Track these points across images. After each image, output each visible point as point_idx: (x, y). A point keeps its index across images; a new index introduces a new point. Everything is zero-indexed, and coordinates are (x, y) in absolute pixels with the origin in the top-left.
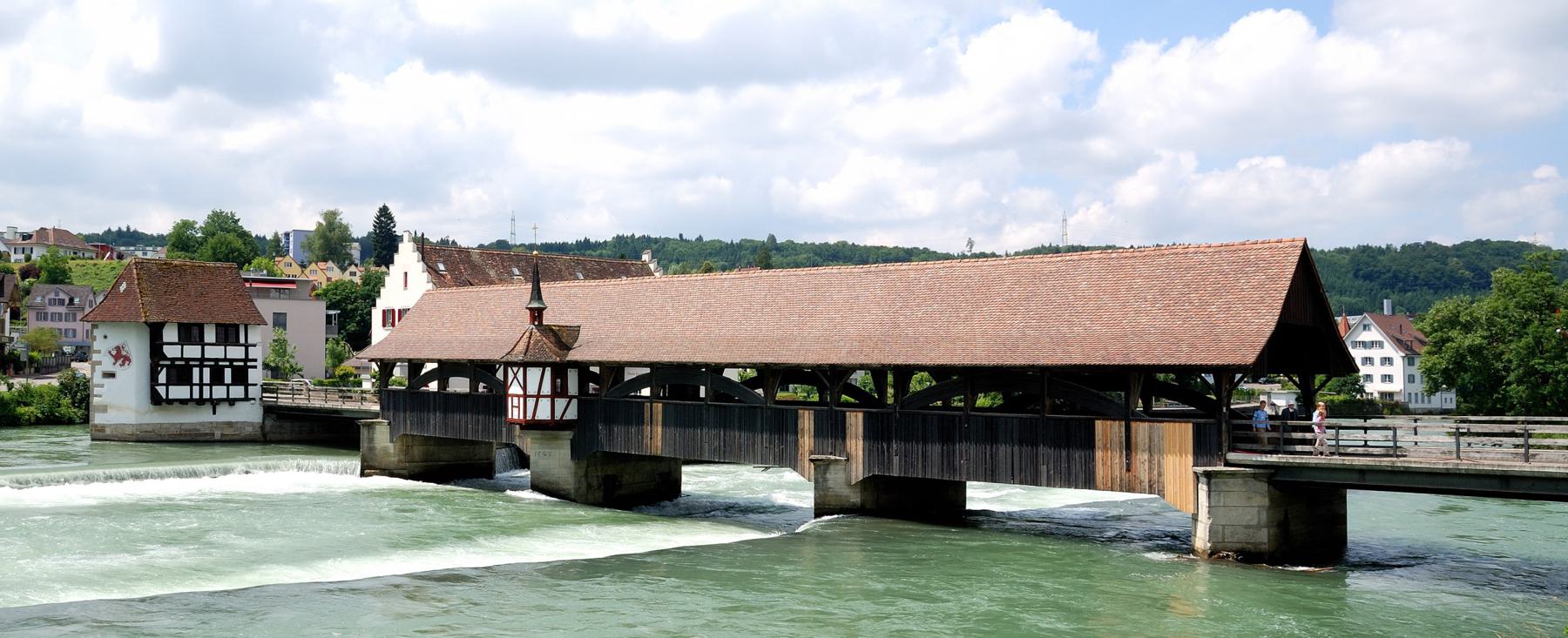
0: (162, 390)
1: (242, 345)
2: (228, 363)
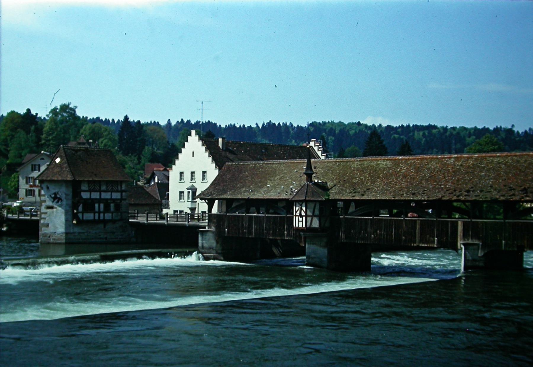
2: (112, 201)
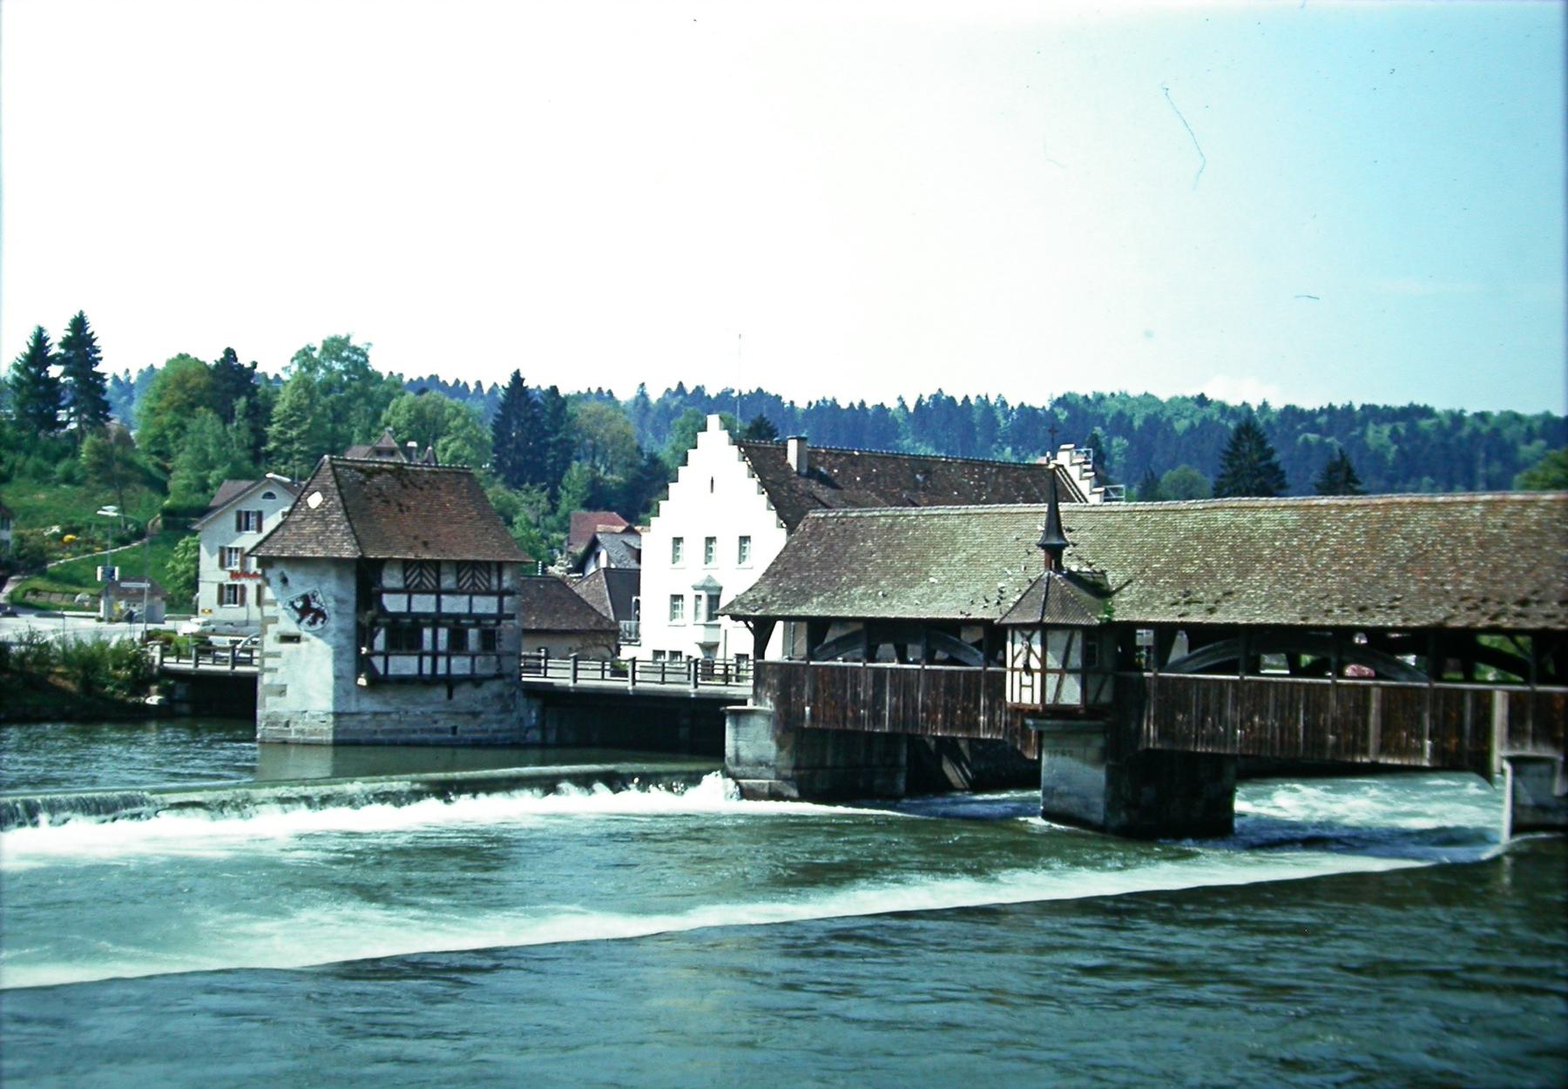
2: (472, 622)
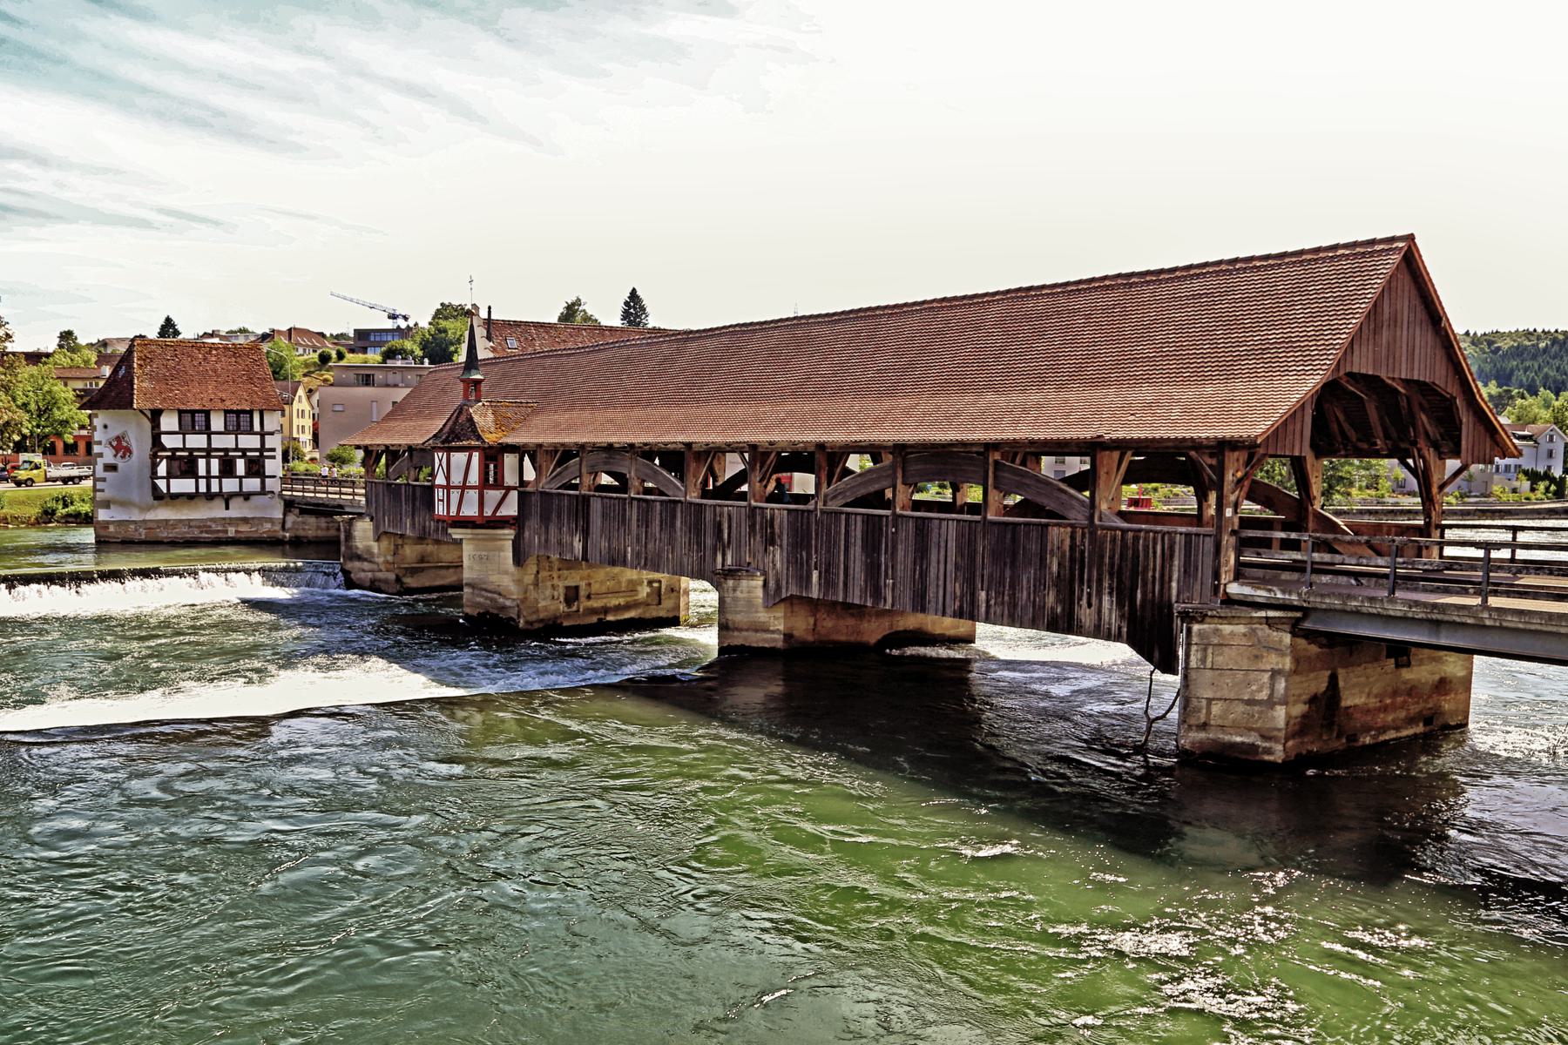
0: (162, 484)
1: (256, 433)
2: (240, 454)
